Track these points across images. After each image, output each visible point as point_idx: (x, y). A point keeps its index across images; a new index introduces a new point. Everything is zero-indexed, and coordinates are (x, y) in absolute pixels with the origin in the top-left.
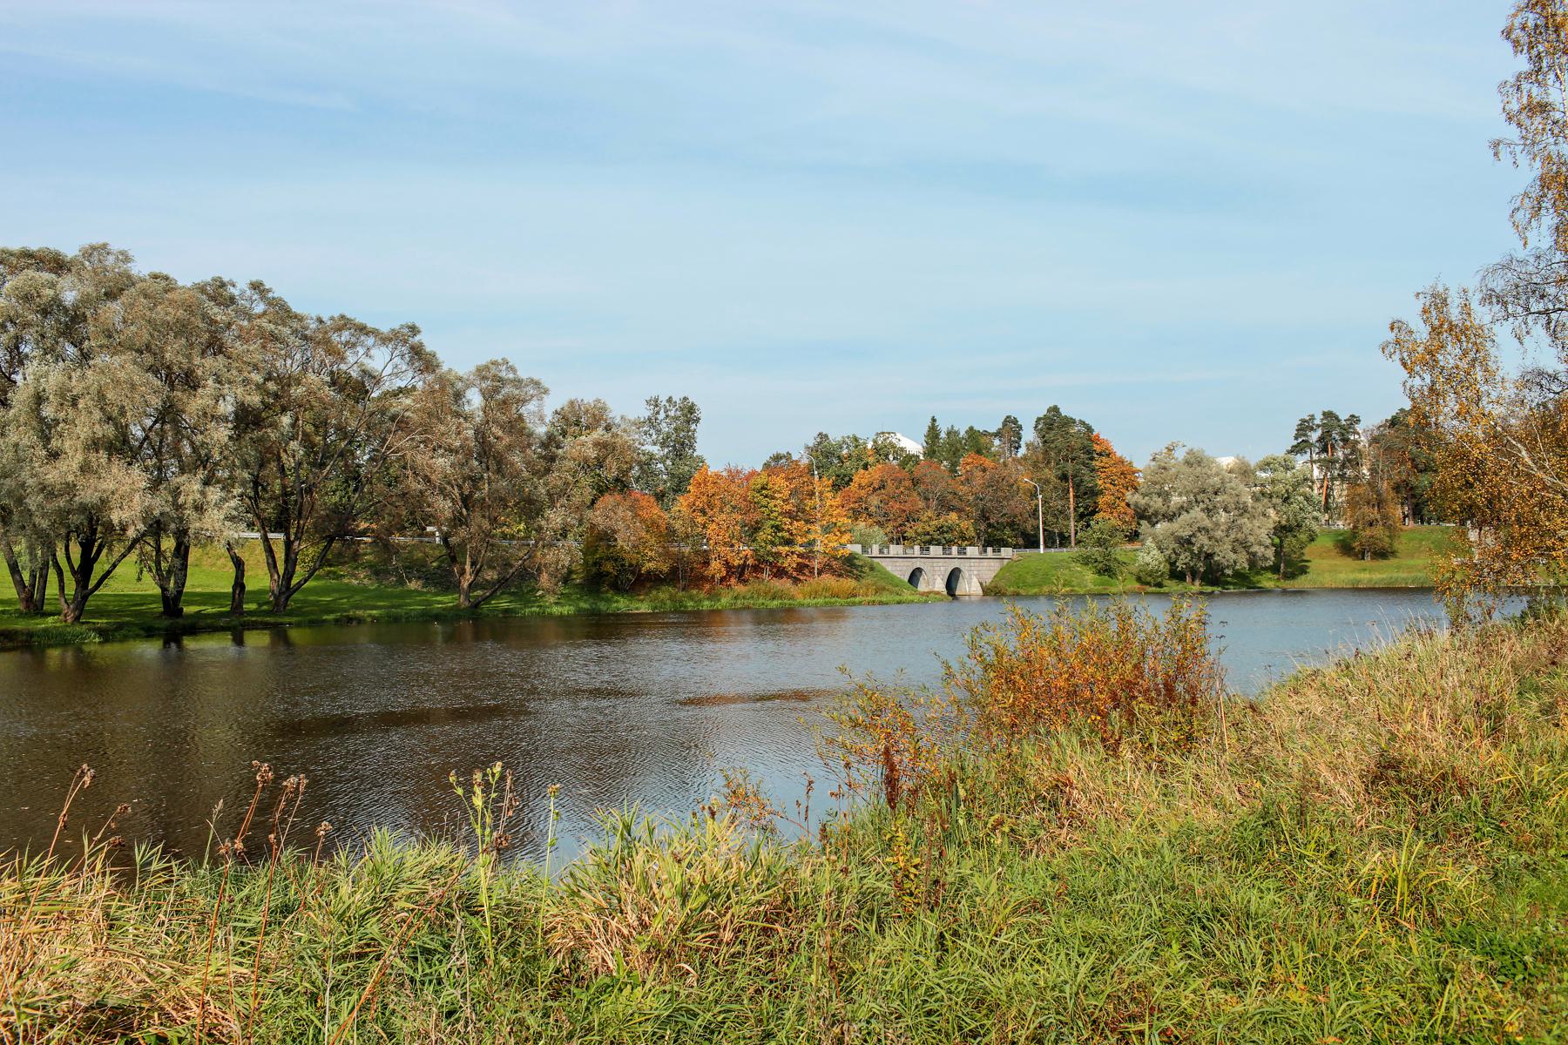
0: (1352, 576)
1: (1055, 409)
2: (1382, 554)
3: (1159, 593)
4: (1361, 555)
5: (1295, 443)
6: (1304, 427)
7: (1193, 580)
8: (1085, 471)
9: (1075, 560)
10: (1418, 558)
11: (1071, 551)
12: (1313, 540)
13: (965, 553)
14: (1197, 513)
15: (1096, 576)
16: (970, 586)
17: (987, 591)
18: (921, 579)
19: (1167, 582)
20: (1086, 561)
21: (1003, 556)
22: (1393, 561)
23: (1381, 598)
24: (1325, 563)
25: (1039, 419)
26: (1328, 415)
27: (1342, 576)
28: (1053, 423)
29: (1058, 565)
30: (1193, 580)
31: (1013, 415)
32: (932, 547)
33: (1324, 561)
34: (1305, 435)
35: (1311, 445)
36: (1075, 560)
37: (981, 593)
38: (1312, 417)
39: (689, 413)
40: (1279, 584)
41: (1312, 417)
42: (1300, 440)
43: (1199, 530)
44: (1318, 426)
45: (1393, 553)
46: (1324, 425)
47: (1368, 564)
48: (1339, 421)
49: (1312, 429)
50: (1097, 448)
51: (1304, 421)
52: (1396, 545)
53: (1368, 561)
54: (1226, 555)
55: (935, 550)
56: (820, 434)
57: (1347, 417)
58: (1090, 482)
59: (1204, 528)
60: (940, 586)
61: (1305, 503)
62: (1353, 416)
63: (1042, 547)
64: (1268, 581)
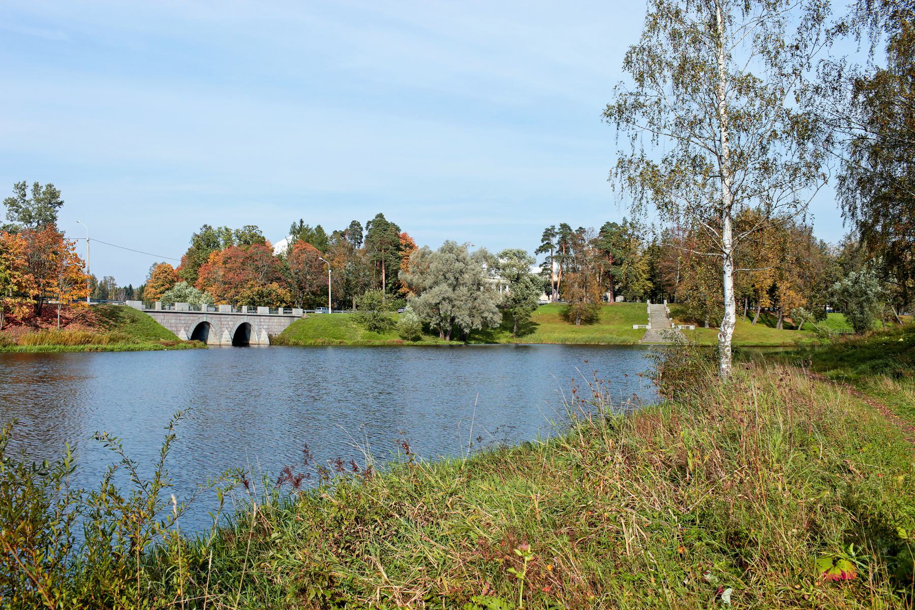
0: (563, 336)
1: (381, 216)
2: (590, 320)
3: (518, 348)
4: (573, 322)
5: (542, 244)
6: (548, 234)
7: (445, 336)
8: (392, 258)
9: (354, 320)
10: (613, 324)
11: (354, 313)
12: (534, 309)
13: (277, 313)
14: (444, 289)
15: (368, 332)
16: (259, 337)
17: (272, 341)
18: (210, 330)
19: (423, 337)
20: (362, 321)
21: (294, 314)
22: (595, 326)
23: (498, 351)
24: (549, 326)
25: (369, 223)
26: (564, 226)
27: (556, 335)
28: (380, 223)
29: (337, 324)
30: (445, 336)
31: (358, 220)
32: (259, 308)
33: (549, 325)
34: (548, 239)
35: (552, 247)
36: (354, 320)
37: (268, 342)
38: (553, 228)
39: (52, 198)
40: (511, 340)
41: (553, 228)
42: (545, 242)
43: (444, 299)
44: (557, 233)
45: (597, 320)
46: (561, 233)
47: (578, 327)
48: (571, 230)
49: (553, 236)
50: (402, 241)
51: (548, 230)
52: (600, 316)
53: (577, 326)
54: (463, 319)
55: (263, 310)
56: (205, 226)
57: (577, 228)
58: (394, 266)
59: (448, 298)
60: (227, 338)
61: (531, 283)
62: (580, 228)
63: (330, 309)
64: (504, 338)
